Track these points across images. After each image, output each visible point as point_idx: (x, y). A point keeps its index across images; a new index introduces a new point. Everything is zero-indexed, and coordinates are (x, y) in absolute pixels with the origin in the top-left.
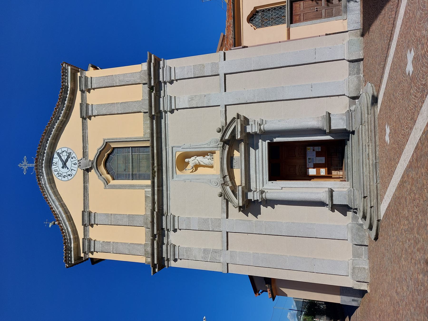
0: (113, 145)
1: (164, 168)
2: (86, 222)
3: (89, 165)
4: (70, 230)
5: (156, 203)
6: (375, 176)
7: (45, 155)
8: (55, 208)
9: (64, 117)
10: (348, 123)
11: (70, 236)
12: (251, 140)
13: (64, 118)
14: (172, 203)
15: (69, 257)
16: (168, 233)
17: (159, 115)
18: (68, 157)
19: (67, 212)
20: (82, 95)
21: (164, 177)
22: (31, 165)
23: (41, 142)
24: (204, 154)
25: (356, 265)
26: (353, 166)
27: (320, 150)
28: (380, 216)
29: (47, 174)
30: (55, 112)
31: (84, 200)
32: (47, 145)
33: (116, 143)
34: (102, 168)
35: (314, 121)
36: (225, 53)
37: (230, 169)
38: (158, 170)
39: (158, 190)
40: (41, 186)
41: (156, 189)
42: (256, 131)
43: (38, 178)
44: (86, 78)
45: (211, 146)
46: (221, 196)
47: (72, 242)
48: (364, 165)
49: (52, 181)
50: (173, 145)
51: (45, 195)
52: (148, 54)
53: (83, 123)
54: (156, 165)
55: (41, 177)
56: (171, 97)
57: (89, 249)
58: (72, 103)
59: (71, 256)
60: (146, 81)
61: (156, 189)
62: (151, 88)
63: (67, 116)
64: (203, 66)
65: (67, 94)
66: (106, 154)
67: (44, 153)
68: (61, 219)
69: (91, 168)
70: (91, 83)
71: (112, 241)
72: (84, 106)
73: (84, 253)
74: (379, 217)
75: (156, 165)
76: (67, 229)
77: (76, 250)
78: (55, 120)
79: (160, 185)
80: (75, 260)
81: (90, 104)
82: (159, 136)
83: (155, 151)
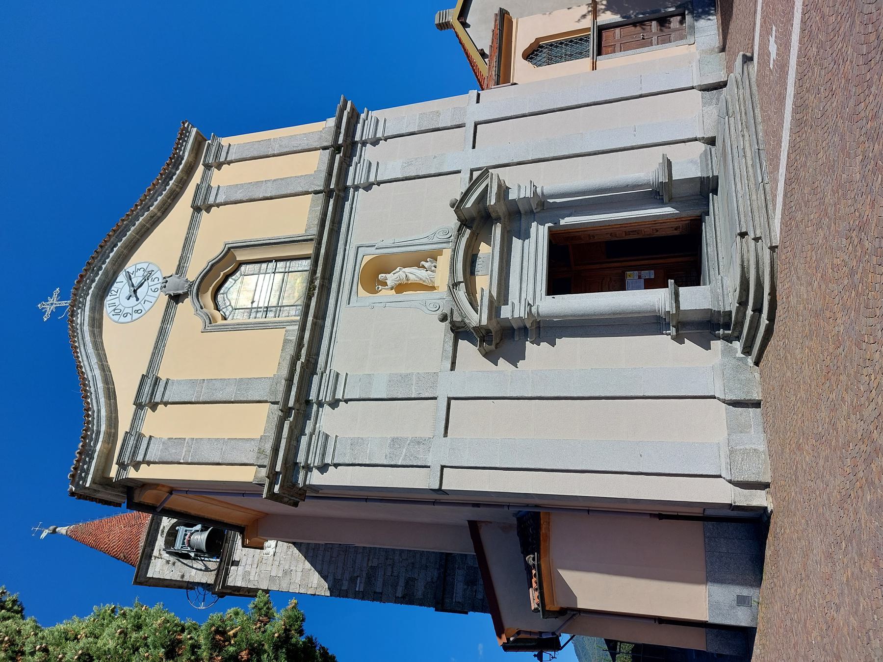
0: (241, 256)
1: (334, 286)
2: (144, 399)
3: (183, 288)
4: (103, 413)
5: (306, 346)
6: (759, 171)
7: (100, 273)
8: (86, 369)
9: (159, 208)
10: (704, 164)
11: (99, 426)
12: (516, 217)
13: (159, 210)
14: (336, 350)
15: (83, 470)
16: (318, 411)
17: (342, 194)
18: (146, 279)
19: (108, 381)
20: (204, 172)
21: (332, 301)
22: (63, 303)
23: (101, 247)
24: (416, 260)
25: (737, 444)
26: (719, 249)
27: (653, 277)
28: (776, 239)
29: (93, 309)
30: (146, 196)
31: (153, 354)
32: (111, 255)
33: (248, 250)
34: (208, 298)
35: (642, 170)
36: (479, 95)
37: (468, 275)
38: (322, 286)
39: (314, 324)
40: (72, 327)
41: (310, 319)
42: (522, 315)
43: (73, 311)
44: (220, 147)
45: (436, 240)
46: (444, 319)
47: (101, 440)
48: (738, 180)
49: (97, 324)
50: (360, 244)
51: (75, 342)
52: (342, 98)
53: (193, 217)
54: (319, 274)
55: (79, 311)
56: (327, 436)
57: (133, 456)
58: (181, 188)
59: (89, 469)
60: (280, 397)
61: (310, 319)
62: (286, 412)
63: (166, 209)
64: (438, 113)
65: (177, 169)
66: (222, 274)
67: (100, 268)
68: (92, 389)
69: (186, 295)
70: (227, 153)
71: (187, 437)
72: (204, 189)
73: (122, 466)
74: (774, 241)
75: (319, 274)
76: (99, 411)
77: (103, 460)
78: (141, 210)
79: (321, 315)
80: (93, 481)
81: (164, 379)
82: (336, 229)
83: (323, 251)
